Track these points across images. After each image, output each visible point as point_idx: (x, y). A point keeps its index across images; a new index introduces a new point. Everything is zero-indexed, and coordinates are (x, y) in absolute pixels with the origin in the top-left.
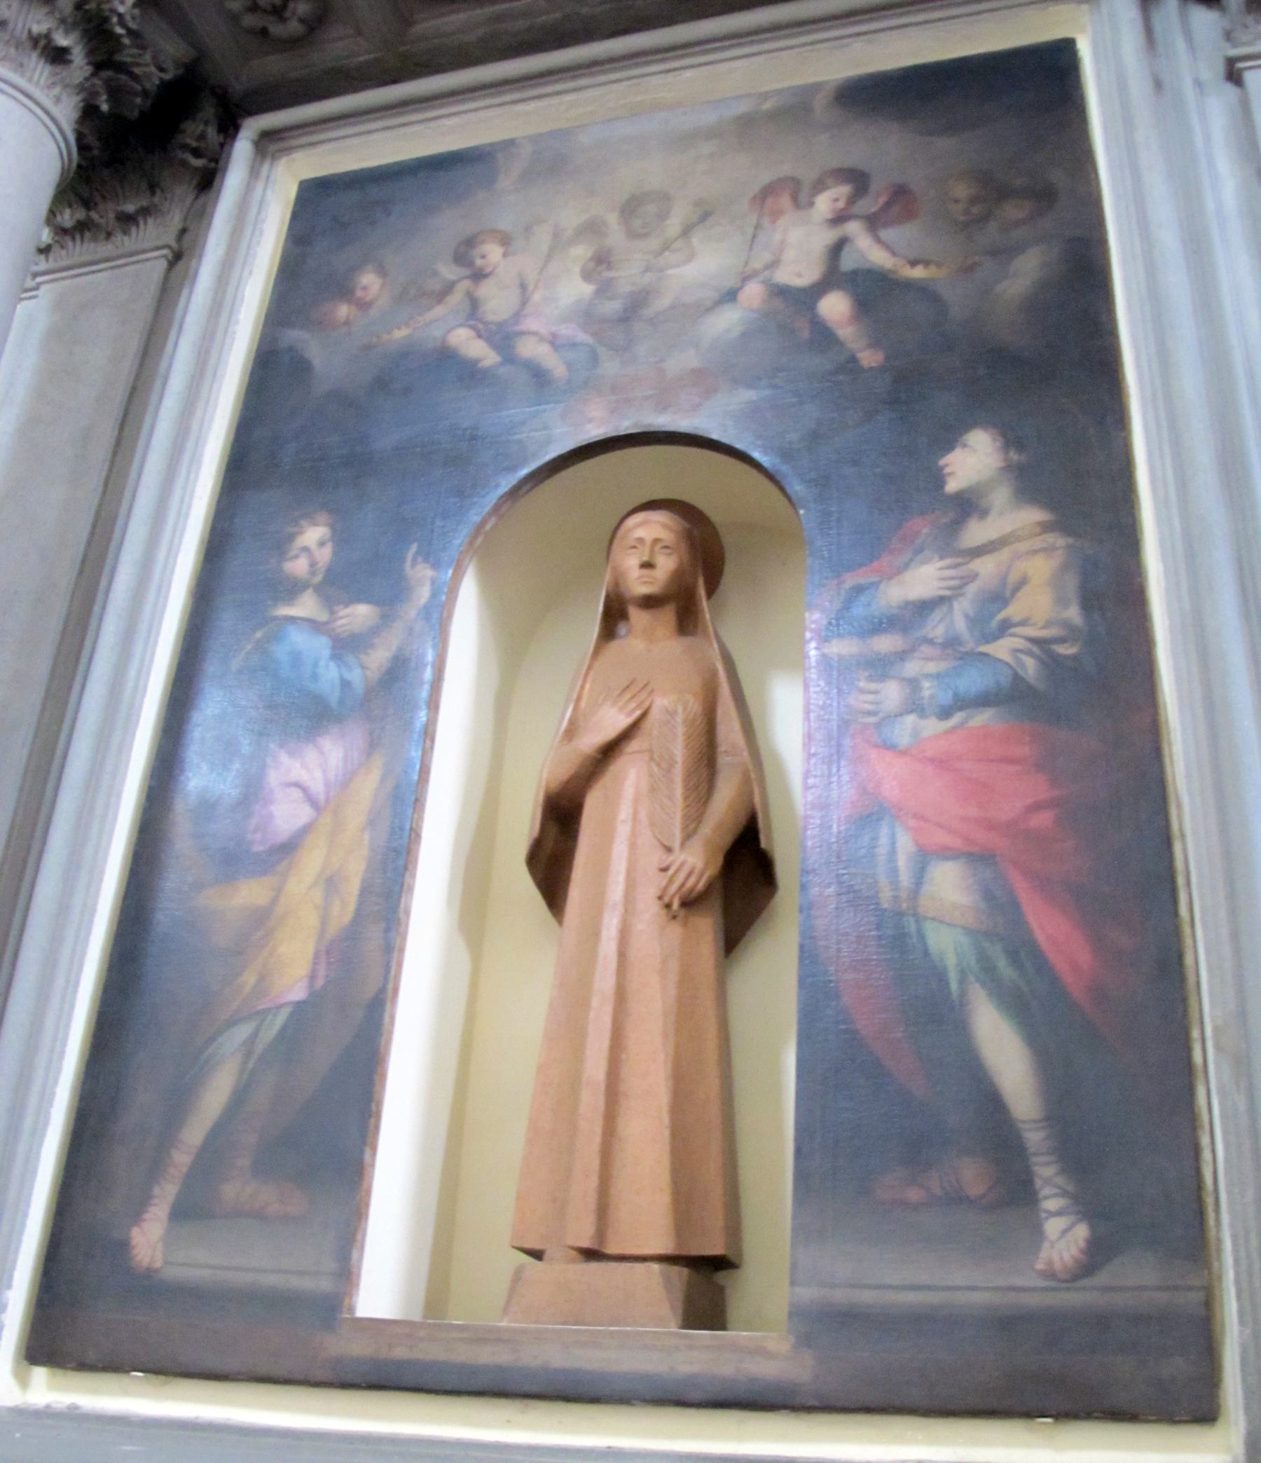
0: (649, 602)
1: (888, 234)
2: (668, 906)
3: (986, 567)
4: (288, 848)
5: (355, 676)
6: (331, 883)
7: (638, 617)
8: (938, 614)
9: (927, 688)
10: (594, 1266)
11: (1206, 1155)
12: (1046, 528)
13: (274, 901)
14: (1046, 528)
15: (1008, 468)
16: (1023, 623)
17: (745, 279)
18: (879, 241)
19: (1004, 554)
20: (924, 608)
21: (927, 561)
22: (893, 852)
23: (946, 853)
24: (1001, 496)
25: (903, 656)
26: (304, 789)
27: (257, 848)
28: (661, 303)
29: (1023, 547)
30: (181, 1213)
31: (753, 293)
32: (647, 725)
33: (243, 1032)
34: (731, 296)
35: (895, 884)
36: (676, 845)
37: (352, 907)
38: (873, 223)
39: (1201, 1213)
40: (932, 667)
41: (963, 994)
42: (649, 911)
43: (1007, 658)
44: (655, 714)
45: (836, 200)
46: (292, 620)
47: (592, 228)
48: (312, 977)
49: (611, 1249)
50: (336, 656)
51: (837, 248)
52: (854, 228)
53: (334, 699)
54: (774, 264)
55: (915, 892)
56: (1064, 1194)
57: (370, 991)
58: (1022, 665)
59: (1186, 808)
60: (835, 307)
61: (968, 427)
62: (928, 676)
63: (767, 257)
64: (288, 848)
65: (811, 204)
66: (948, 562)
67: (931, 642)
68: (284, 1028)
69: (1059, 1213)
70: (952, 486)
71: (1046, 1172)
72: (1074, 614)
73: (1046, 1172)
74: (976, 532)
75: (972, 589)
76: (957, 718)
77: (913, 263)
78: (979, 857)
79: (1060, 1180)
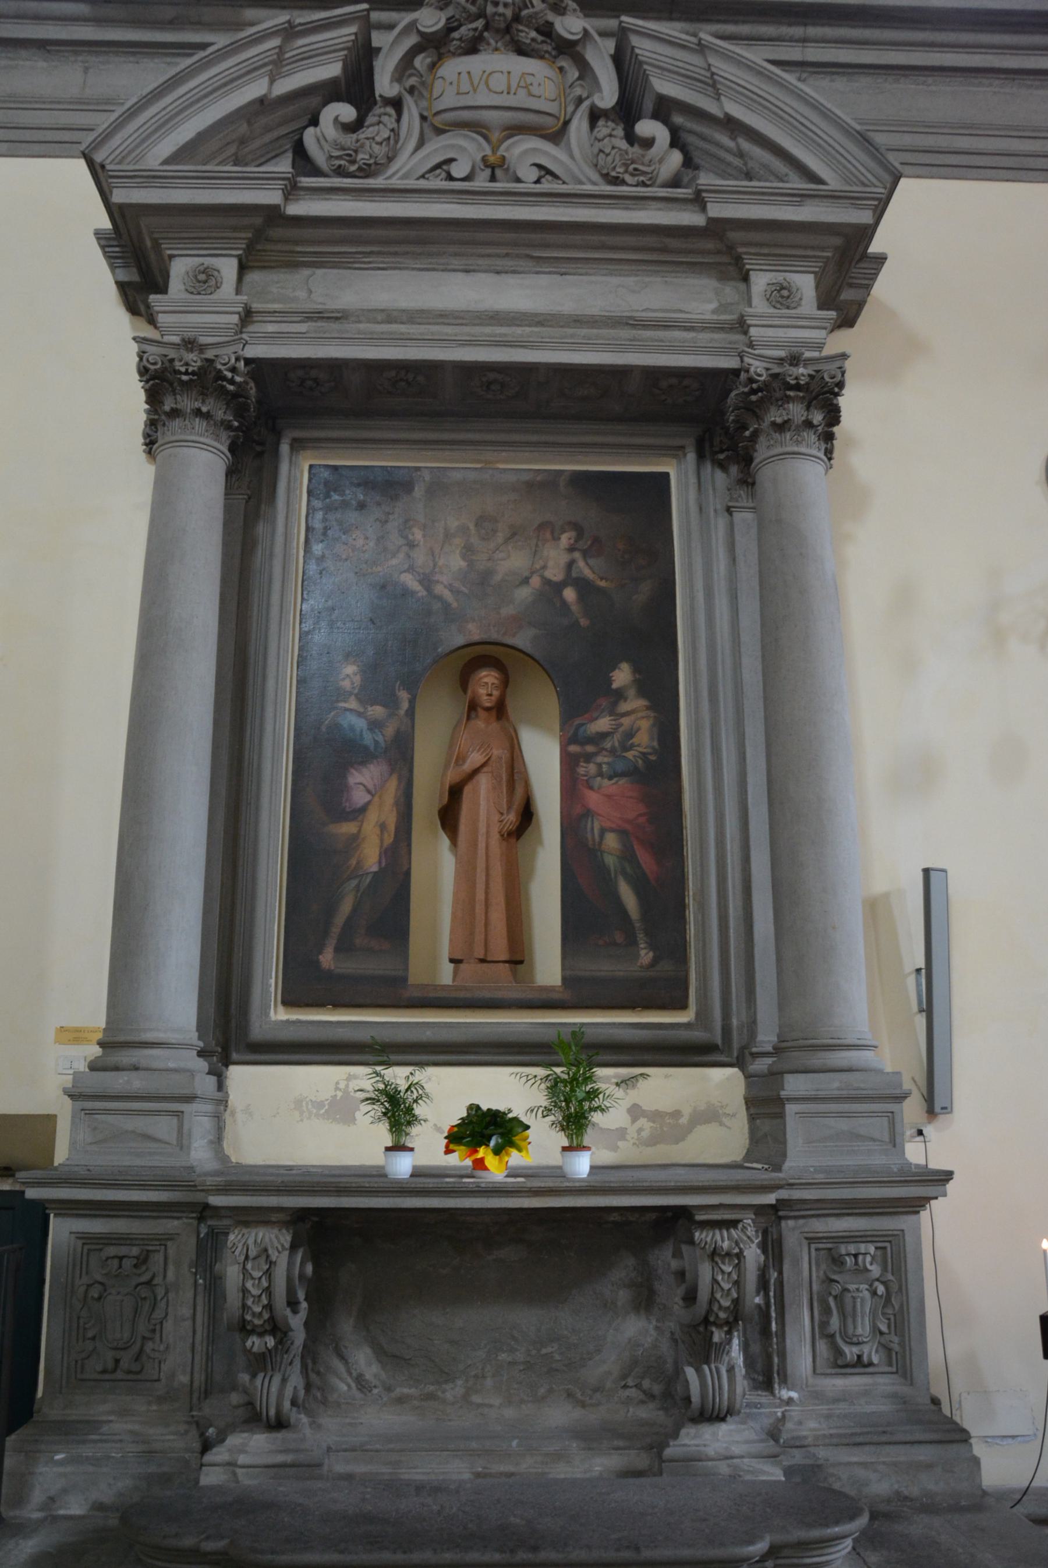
0: (488, 709)
1: (591, 562)
2: (502, 836)
3: (626, 721)
4: (363, 809)
5: (380, 738)
6: (383, 827)
7: (482, 713)
8: (609, 738)
9: (605, 768)
10: (485, 965)
11: (688, 931)
12: (648, 708)
13: (359, 831)
14: (648, 708)
15: (635, 681)
16: (638, 745)
17: (532, 573)
18: (587, 564)
19: (633, 717)
20: (603, 736)
21: (604, 717)
22: (592, 829)
23: (612, 830)
24: (632, 692)
25: (596, 754)
26: (364, 786)
27: (348, 810)
28: (498, 578)
29: (640, 714)
30: (337, 950)
31: (536, 581)
32: (490, 762)
33: (354, 883)
34: (526, 581)
35: (594, 840)
36: (505, 812)
37: (392, 836)
38: (585, 554)
39: (686, 950)
40: (606, 760)
41: (616, 877)
42: (495, 837)
43: (631, 758)
44: (493, 759)
45: (570, 539)
46: (346, 710)
47: (464, 530)
48: (380, 862)
49: (489, 959)
50: (370, 729)
51: (570, 565)
52: (577, 555)
53: (372, 748)
54: (544, 567)
55: (600, 843)
56: (646, 943)
57: (405, 869)
58: (637, 761)
59: (688, 817)
60: (570, 594)
61: (621, 661)
62: (604, 763)
63: (541, 563)
64: (363, 809)
65: (560, 539)
66: (612, 718)
67: (606, 750)
68: (370, 882)
69: (645, 948)
70: (614, 686)
71: (641, 936)
72: (655, 744)
73: (641, 936)
74: (624, 707)
75: (621, 729)
76: (615, 780)
77: (602, 579)
78: (622, 833)
79: (645, 938)
